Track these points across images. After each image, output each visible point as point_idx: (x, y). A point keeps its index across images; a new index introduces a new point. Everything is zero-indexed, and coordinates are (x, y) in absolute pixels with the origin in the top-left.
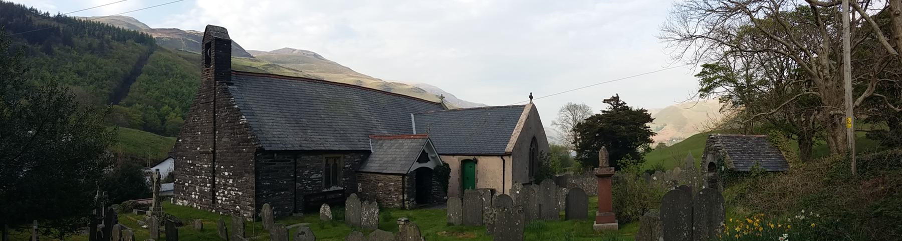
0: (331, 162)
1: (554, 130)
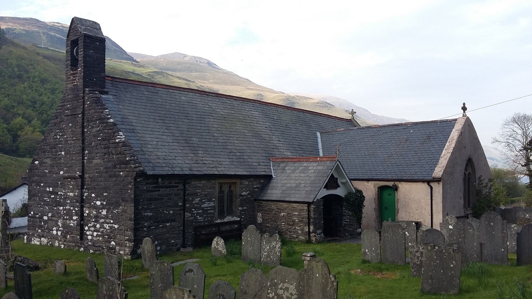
0: (226, 189)
1: (496, 149)
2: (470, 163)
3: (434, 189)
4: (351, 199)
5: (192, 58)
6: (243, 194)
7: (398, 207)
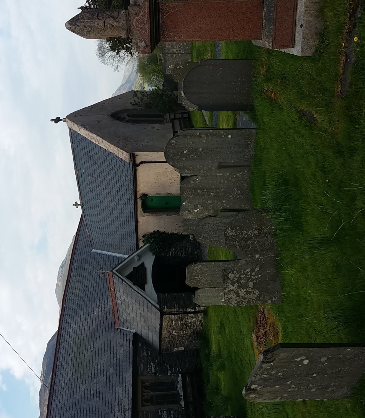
0: (149, 394)
2: (117, 115)
3: (144, 160)
4: (157, 250)
5: (59, 280)
6: (153, 371)
7: (165, 194)
